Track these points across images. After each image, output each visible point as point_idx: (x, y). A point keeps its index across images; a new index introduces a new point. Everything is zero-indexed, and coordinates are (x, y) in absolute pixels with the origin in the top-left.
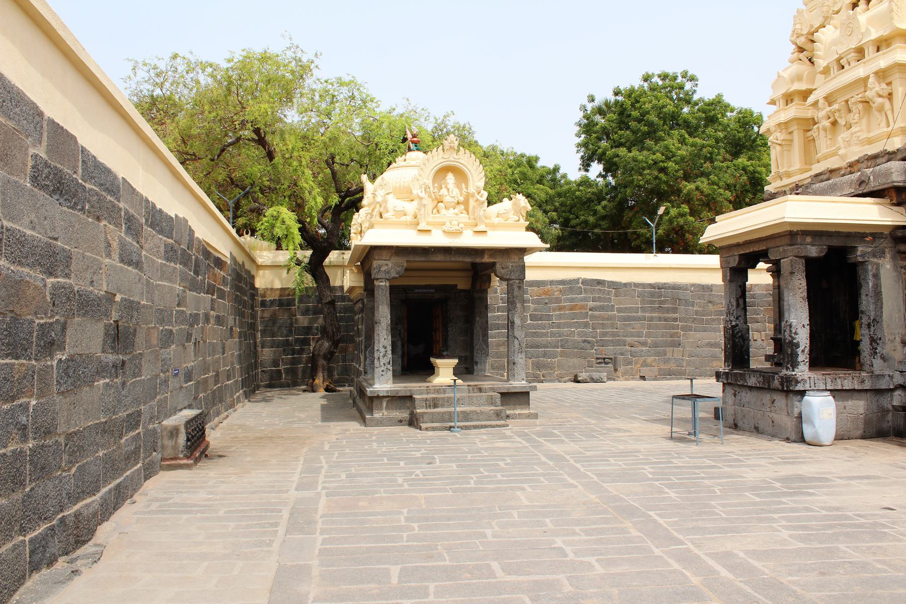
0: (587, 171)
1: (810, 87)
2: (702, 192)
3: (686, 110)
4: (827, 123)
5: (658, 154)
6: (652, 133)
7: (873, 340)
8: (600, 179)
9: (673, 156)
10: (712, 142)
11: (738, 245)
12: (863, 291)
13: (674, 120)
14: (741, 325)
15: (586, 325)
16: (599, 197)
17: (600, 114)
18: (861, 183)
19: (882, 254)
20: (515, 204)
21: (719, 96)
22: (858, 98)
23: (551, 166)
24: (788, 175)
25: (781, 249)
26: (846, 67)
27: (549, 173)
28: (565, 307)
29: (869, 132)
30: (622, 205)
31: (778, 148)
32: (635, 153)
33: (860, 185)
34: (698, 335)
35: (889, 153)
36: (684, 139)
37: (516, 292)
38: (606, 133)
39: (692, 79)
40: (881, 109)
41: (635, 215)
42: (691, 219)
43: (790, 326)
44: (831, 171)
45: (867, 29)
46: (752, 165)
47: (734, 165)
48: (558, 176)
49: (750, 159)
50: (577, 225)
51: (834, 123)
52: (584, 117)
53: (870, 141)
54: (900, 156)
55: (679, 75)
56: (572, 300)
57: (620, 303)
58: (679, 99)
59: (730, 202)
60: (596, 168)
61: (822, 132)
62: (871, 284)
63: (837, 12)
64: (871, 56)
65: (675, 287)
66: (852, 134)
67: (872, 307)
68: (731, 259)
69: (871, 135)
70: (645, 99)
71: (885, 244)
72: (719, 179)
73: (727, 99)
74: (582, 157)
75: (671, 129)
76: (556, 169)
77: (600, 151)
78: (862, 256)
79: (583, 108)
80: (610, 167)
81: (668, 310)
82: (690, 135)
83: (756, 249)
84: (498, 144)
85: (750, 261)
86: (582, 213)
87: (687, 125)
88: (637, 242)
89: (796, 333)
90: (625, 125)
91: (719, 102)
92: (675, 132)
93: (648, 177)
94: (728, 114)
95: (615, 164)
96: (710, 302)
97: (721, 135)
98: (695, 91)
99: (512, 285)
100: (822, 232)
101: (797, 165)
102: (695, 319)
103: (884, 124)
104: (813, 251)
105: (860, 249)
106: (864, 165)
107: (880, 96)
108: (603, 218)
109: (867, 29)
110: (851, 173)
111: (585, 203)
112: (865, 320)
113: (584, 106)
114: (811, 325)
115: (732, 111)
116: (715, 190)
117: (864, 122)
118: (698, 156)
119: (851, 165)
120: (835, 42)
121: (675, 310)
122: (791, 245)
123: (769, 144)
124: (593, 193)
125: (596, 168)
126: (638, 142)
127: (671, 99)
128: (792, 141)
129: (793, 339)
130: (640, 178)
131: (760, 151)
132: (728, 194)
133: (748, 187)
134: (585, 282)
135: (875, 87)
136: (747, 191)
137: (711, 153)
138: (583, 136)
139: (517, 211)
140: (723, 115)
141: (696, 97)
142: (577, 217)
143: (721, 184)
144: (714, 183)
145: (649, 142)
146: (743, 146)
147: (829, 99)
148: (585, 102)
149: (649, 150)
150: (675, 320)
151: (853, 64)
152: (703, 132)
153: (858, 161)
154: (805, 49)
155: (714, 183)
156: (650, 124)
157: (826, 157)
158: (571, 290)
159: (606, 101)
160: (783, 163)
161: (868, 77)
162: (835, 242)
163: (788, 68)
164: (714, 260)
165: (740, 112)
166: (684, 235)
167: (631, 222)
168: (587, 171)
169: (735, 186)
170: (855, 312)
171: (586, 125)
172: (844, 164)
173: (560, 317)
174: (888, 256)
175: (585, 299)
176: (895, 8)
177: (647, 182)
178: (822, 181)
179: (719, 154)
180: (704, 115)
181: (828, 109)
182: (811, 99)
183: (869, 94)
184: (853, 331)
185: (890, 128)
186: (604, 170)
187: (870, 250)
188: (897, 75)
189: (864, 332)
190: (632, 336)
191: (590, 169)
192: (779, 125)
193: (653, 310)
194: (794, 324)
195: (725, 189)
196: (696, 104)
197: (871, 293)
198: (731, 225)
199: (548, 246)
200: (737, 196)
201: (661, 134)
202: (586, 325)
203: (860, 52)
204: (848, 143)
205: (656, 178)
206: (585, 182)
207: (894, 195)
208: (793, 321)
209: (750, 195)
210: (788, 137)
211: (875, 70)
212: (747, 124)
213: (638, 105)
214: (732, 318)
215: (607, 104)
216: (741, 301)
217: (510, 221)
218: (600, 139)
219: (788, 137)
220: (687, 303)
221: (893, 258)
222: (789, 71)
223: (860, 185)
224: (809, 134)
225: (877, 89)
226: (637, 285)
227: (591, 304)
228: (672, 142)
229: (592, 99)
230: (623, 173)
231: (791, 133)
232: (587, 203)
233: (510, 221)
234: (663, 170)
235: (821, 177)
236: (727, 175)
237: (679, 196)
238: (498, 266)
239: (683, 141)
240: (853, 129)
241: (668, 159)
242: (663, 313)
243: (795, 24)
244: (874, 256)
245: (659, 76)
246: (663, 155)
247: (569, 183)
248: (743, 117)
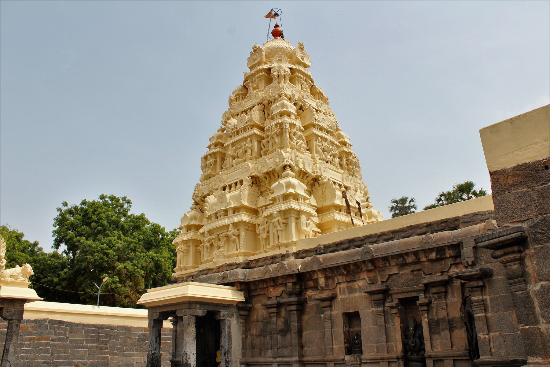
0: (57, 248)
1: (200, 224)
2: (127, 270)
3: (123, 220)
4: (208, 244)
5: (105, 245)
6: (103, 232)
7: (227, 362)
8: (65, 255)
9: (114, 246)
10: (136, 240)
11: (159, 307)
12: (223, 335)
13: (116, 225)
14: (157, 353)
15: (47, 351)
16: (63, 266)
17: (70, 214)
18: (224, 278)
19: (231, 316)
20: (23, 270)
21: (143, 215)
22: (224, 234)
23: (32, 242)
24: (186, 269)
25: (184, 311)
26: (219, 218)
27: (30, 245)
28: (34, 338)
29: (228, 252)
30: (77, 273)
31: (182, 253)
32: (90, 242)
33: (223, 279)
34: (120, 358)
35: (237, 264)
36: (121, 237)
37: (14, 328)
38: (73, 227)
39: (129, 202)
40: (234, 241)
41: (84, 280)
42: (119, 285)
43: (186, 354)
44: (209, 270)
45: (230, 202)
46: (157, 256)
47: (147, 255)
48: (36, 249)
49: (156, 253)
50: (45, 282)
51: (212, 245)
52: (60, 215)
53: (228, 257)
54: (242, 266)
55: (121, 199)
56: (40, 334)
57: (72, 336)
58: (119, 213)
59: (143, 277)
60: (63, 247)
61: (205, 248)
62: (226, 331)
63: (216, 190)
64: (231, 215)
65: (108, 327)
66: (220, 252)
67: (227, 344)
68: (155, 314)
69: (229, 253)
70: (101, 210)
71: (234, 310)
72: (138, 263)
73: (147, 217)
74: (55, 240)
75: (114, 230)
76: (36, 244)
77: (68, 237)
78: (223, 316)
79: (59, 210)
80: (72, 247)
81: (103, 342)
82: (124, 234)
83: (170, 310)
84: (7, 226)
85: (165, 316)
86: (50, 274)
87: (122, 228)
88: (84, 297)
89: (189, 358)
90: (82, 223)
91: (142, 218)
92: (115, 232)
93: (97, 257)
94: (146, 225)
95: (77, 247)
96: (129, 337)
97: (142, 237)
98: (129, 210)
99: (12, 324)
100: (205, 302)
101: (190, 264)
102: (119, 348)
103: (235, 249)
104: (200, 313)
105: (223, 312)
106: (225, 269)
107: (234, 235)
108: (64, 279)
109: (230, 202)
110: (218, 272)
111: (53, 269)
112: (223, 351)
113: (60, 209)
114: (197, 353)
115: (148, 224)
116: (135, 269)
117: (226, 246)
118: (128, 248)
119: (219, 268)
120: (215, 204)
121: (107, 342)
122: (189, 309)
123: (177, 251)
124: (59, 263)
125: (63, 247)
126: (94, 235)
127: (116, 212)
128: (189, 250)
129: (188, 361)
130: (91, 257)
131: (161, 249)
132: (142, 272)
133: (154, 269)
134: (51, 321)
135: (232, 231)
136: (153, 271)
137: (135, 247)
138: (58, 227)
139: (24, 274)
140: (144, 226)
141: (129, 213)
142: (46, 277)
143: (139, 266)
144: (135, 265)
145: (100, 236)
146: (153, 245)
147: (210, 232)
148: (61, 206)
149: (99, 241)
150: (107, 348)
151: (222, 217)
152: (132, 234)
153: (222, 266)
154: (199, 203)
155: (135, 265)
156: (103, 226)
157: (206, 262)
158: (40, 327)
159: (76, 206)
160: (185, 263)
161: (229, 225)
162: (211, 308)
163: (190, 212)
164: (144, 313)
165: (153, 225)
166: (114, 295)
167: (81, 284)
168: (57, 248)
169: (146, 268)
170: (218, 346)
171: (61, 220)
172: (215, 267)
173: (29, 345)
174: (235, 317)
175: (49, 333)
176: (242, 195)
177: (95, 260)
178: (204, 274)
179: (139, 248)
180: (133, 224)
181: (209, 237)
182: (201, 231)
183: (229, 233)
184: (215, 356)
185: (238, 252)
186: (68, 249)
187: (227, 313)
188: (242, 227)
189: (222, 357)
190: (77, 359)
191: (60, 247)
192: (183, 241)
193: (93, 342)
194: (188, 353)
195: (141, 269)
196: (129, 217)
197: (227, 336)
198: (154, 295)
199: (43, 299)
200: (147, 274)
201: (108, 232)
202: (47, 351)
203: (226, 212)
204: (218, 257)
205: (101, 258)
206: (55, 256)
207: (239, 285)
208: (188, 351)
209: (154, 274)
210: (187, 248)
211: (233, 222)
212: (156, 232)
213: (96, 213)
214: (152, 349)
215: (76, 208)
216: (158, 339)
217: (19, 280)
218: (68, 229)
219: (187, 248)
220: (115, 338)
221: (237, 318)
222: (191, 213)
223: (223, 279)
224: (198, 248)
225: (233, 231)
226: (84, 325)
227: (53, 336)
228: (113, 239)
229: (65, 204)
230: (81, 253)
231: (189, 246)
232: (54, 269)
233: (19, 280)
234: (107, 254)
235: (203, 272)
236: (142, 261)
237: (113, 270)
238: (4, 310)
239: (119, 238)
240: (221, 250)
241: (110, 248)
242: (99, 344)
243: (195, 191)
244: (229, 317)
245: (109, 198)
246: (107, 245)
247: (43, 254)
248: (155, 229)
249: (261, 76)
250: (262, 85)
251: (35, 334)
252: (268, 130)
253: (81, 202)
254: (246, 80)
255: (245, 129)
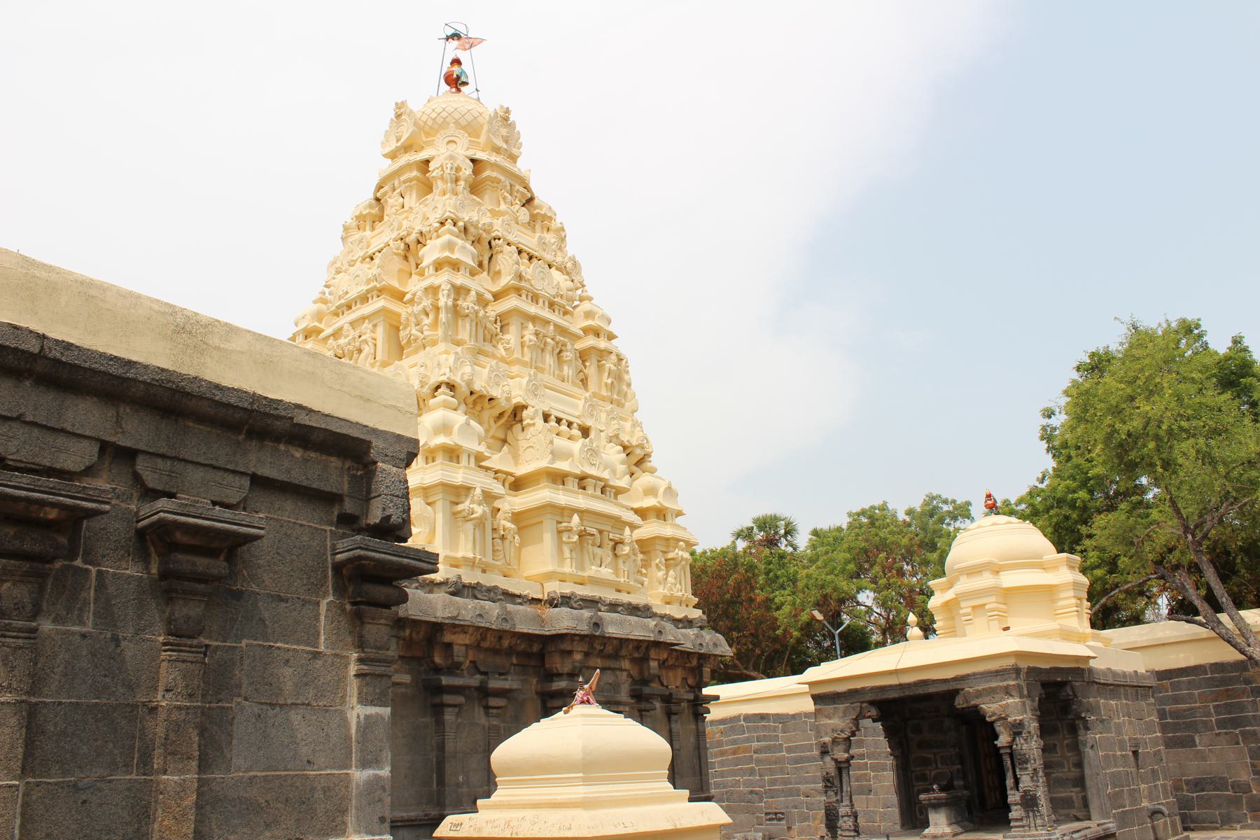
56: (734, 742)
57: (789, 740)
134: (748, 718)
158: (733, 730)
175: (748, 740)
227: (755, 744)
249: (410, 180)
250: (411, 200)
251: (728, 743)
252: (411, 301)
253: (906, 507)
254: (379, 187)
255: (364, 298)
